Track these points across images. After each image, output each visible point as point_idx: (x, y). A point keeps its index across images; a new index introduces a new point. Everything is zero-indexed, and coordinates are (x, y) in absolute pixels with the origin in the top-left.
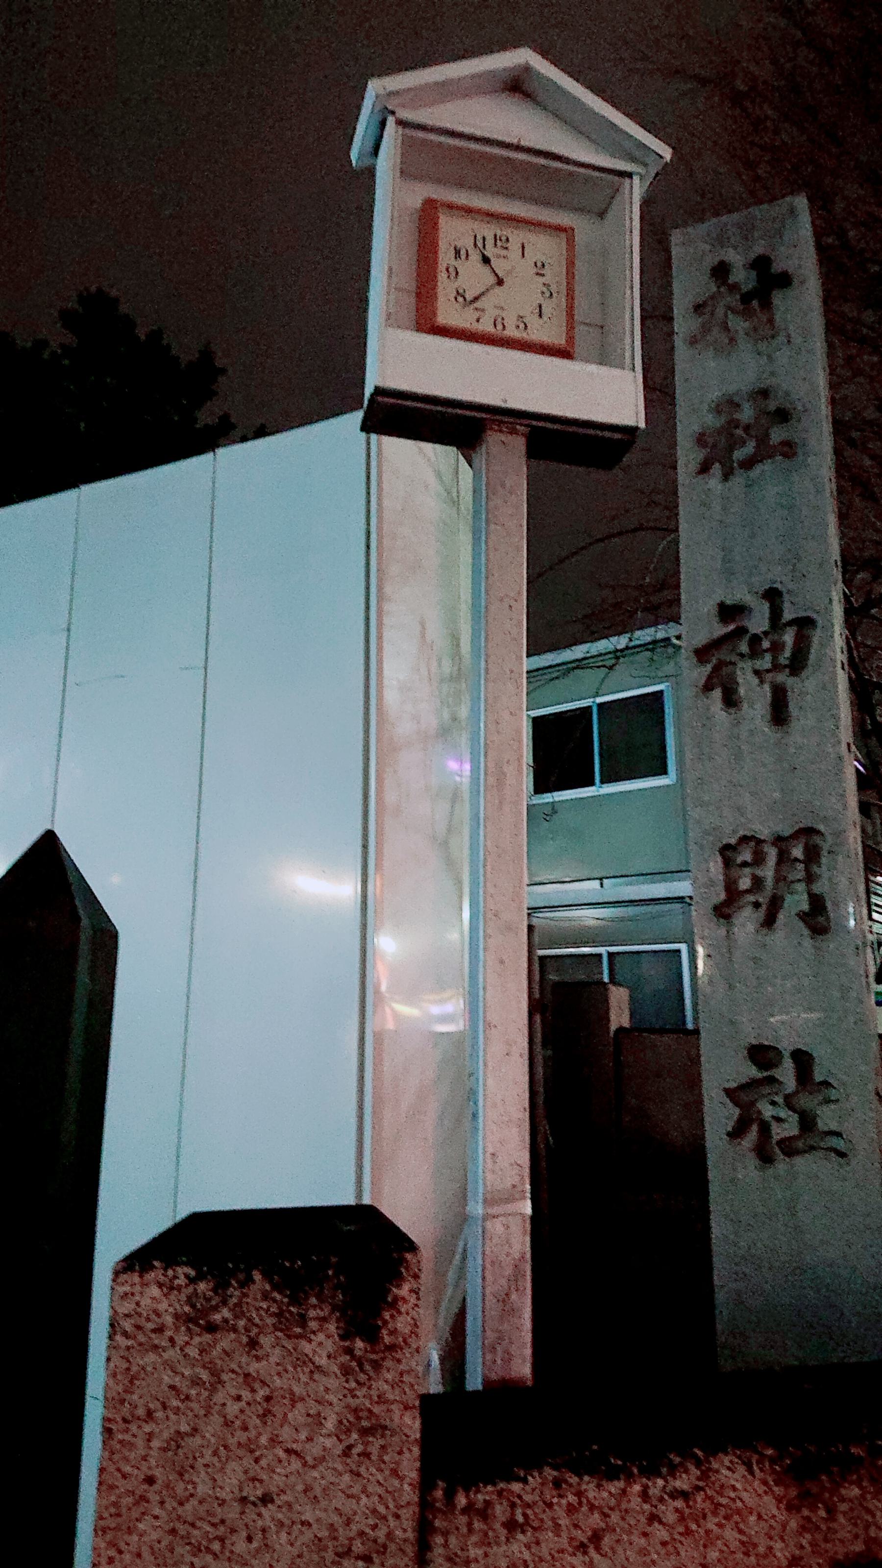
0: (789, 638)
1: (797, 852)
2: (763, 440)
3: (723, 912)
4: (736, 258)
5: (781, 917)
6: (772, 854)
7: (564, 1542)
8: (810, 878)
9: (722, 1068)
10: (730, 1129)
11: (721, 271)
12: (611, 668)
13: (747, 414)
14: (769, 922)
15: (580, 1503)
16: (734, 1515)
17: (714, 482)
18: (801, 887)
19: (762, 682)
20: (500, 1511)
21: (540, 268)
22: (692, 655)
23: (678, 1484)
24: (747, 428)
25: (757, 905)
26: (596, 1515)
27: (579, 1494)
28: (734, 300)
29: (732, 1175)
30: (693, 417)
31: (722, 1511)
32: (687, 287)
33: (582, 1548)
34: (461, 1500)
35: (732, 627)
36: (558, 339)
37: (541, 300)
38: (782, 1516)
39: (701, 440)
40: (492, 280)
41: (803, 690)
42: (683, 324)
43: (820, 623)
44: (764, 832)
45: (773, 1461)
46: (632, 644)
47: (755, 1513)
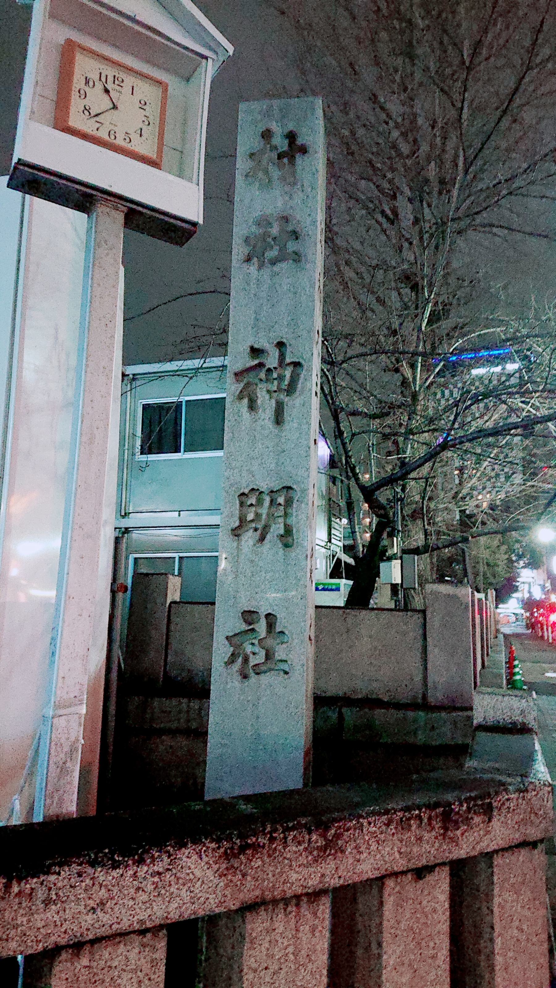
0: (288, 373)
1: (281, 500)
2: (282, 249)
3: (236, 533)
4: (275, 127)
5: (268, 537)
6: (267, 499)
8: (286, 515)
9: (226, 622)
10: (226, 660)
11: (267, 135)
12: (191, 378)
13: (275, 230)
14: (262, 539)
16: (189, 882)
17: (253, 269)
18: (281, 520)
20: (41, 894)
21: (143, 105)
22: (233, 376)
23: (156, 868)
24: (274, 239)
25: (256, 530)
26: (103, 890)
28: (274, 155)
29: (224, 685)
30: (242, 227)
31: (181, 881)
32: (247, 141)
34: (16, 889)
35: (256, 362)
36: (154, 156)
37: (141, 125)
38: (216, 881)
39: (247, 240)
40: (112, 106)
41: (294, 404)
42: (242, 164)
43: (305, 367)
44: (264, 486)
46: (204, 366)
47: (201, 880)
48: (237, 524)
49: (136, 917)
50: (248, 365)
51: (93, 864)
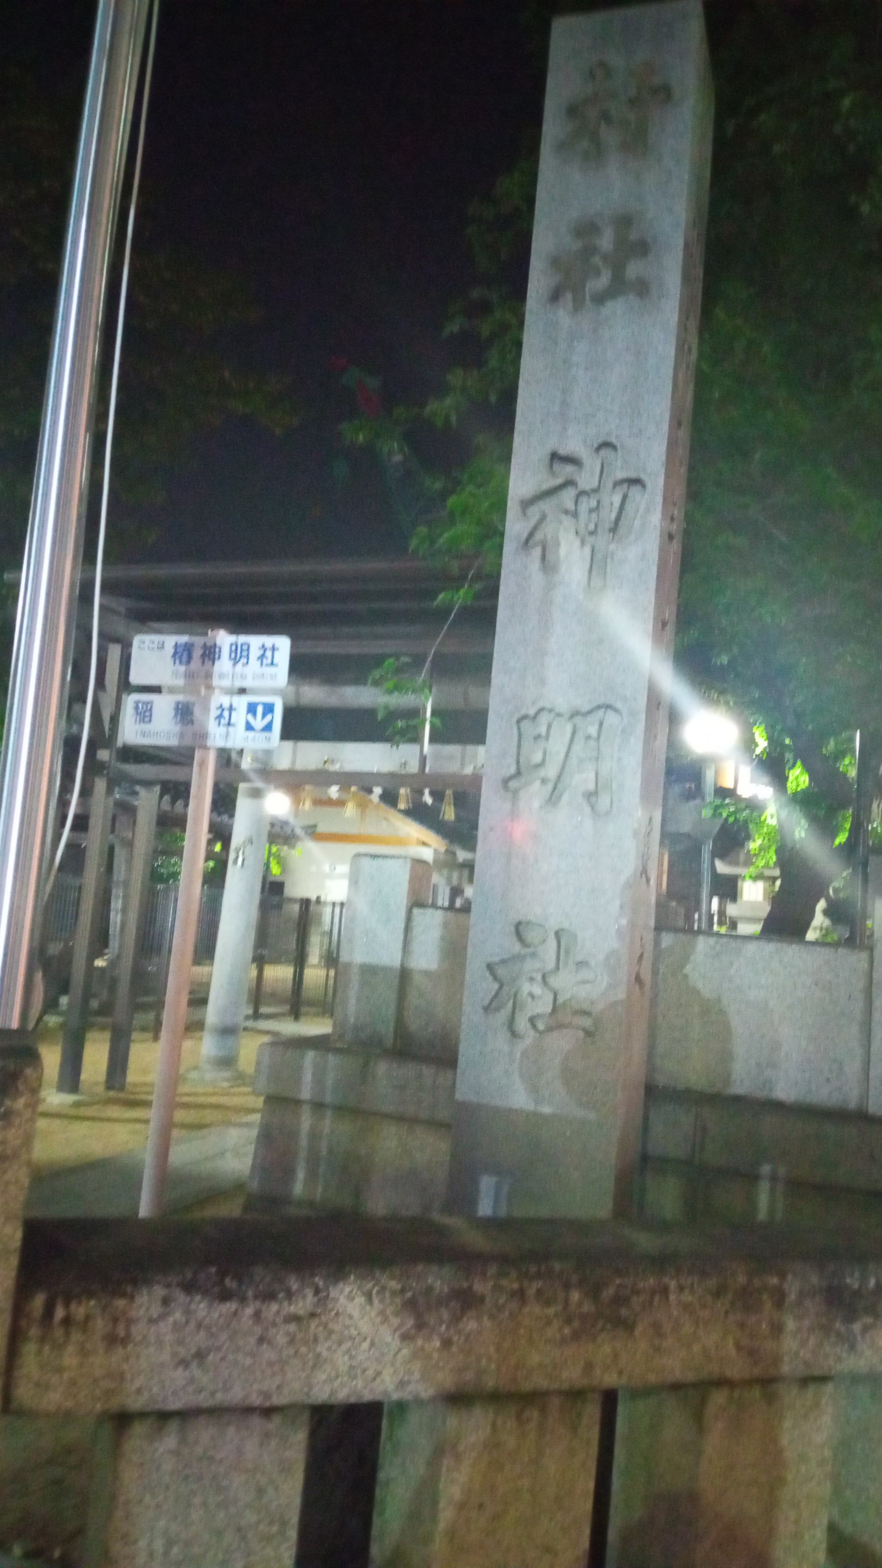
7: (166, 1356)
15: (187, 1322)
19: (583, 543)
20: (100, 1325)
23: (292, 1309)
27: (187, 1312)
33: (184, 1363)
34: (60, 1313)
39: (555, 262)
45: (394, 1293)
47: (368, 1340)
48: (513, 770)
49: (255, 1387)
50: (545, 486)
51: (189, 1288)
